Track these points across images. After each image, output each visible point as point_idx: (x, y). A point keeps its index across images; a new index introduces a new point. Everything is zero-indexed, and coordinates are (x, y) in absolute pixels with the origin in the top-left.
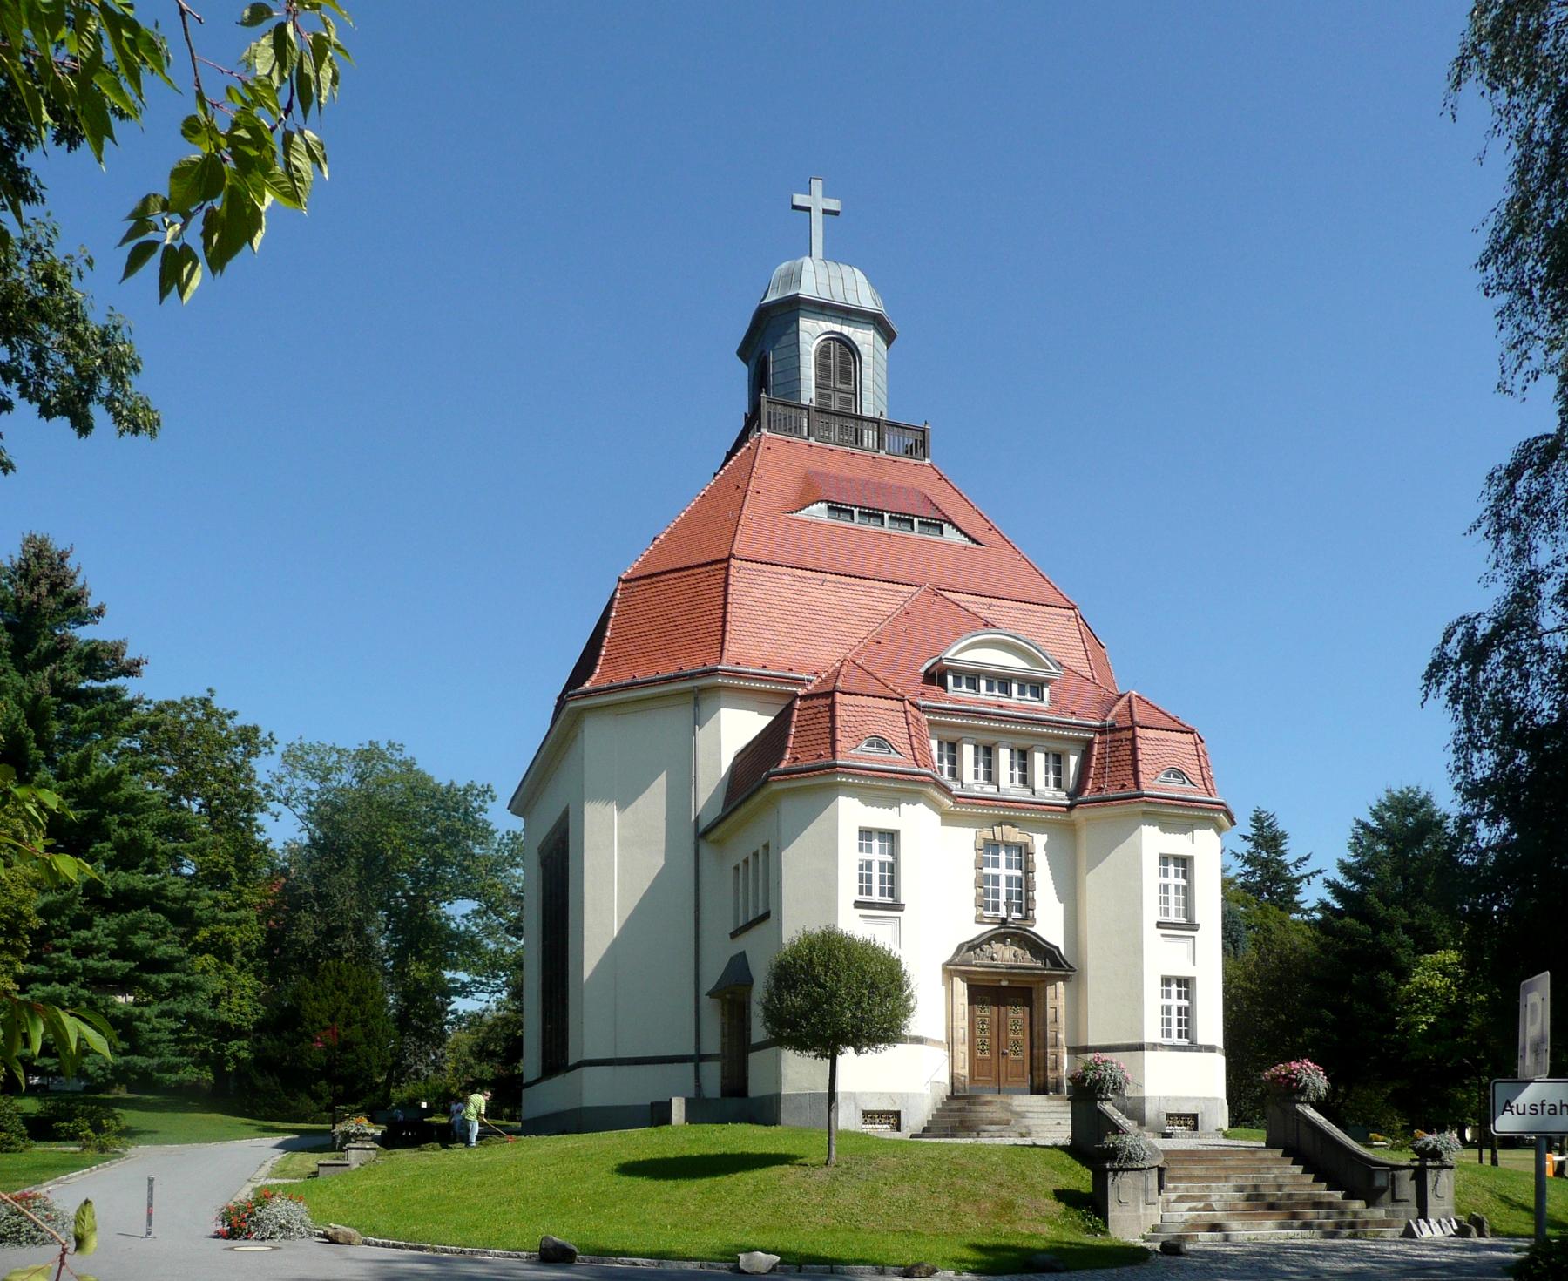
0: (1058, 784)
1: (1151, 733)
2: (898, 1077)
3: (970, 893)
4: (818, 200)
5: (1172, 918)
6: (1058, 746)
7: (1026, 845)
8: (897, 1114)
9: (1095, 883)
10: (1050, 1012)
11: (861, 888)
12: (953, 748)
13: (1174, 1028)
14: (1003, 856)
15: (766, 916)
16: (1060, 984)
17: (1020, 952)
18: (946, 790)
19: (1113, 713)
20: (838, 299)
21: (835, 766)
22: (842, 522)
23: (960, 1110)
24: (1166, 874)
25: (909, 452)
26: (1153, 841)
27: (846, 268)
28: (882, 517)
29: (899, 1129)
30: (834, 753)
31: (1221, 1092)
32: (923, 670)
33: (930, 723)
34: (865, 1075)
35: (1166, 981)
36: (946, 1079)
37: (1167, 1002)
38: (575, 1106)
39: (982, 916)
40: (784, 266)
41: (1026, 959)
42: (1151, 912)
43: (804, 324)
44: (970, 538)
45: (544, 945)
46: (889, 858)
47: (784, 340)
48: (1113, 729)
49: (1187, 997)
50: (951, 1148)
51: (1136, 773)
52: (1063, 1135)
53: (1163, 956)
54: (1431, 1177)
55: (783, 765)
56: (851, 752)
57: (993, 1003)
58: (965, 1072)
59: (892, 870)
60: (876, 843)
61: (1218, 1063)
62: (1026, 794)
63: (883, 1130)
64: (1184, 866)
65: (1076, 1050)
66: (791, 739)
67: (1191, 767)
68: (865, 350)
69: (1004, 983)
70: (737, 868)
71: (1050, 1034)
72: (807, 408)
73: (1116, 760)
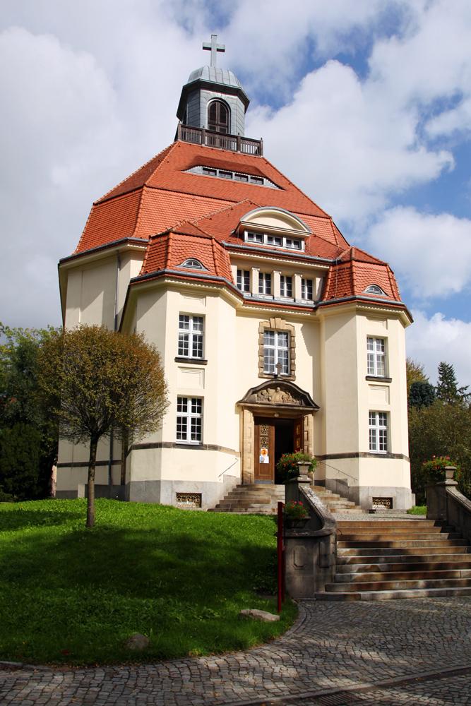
0: (310, 297)
3: (256, 359)
7: (290, 331)
8: (200, 495)
16: (310, 416)
18: (240, 296)
20: (220, 81)
24: (371, 348)
26: (363, 326)
29: (200, 506)
31: (407, 483)
35: (372, 414)
36: (239, 476)
37: (373, 427)
41: (291, 401)
42: (362, 371)
44: (278, 186)
48: (340, 262)
49: (385, 424)
51: (352, 286)
53: (371, 398)
58: (252, 470)
59: (199, 340)
60: (191, 322)
61: (405, 466)
63: (189, 505)
64: (383, 343)
67: (385, 284)
69: (276, 416)
73: (341, 280)
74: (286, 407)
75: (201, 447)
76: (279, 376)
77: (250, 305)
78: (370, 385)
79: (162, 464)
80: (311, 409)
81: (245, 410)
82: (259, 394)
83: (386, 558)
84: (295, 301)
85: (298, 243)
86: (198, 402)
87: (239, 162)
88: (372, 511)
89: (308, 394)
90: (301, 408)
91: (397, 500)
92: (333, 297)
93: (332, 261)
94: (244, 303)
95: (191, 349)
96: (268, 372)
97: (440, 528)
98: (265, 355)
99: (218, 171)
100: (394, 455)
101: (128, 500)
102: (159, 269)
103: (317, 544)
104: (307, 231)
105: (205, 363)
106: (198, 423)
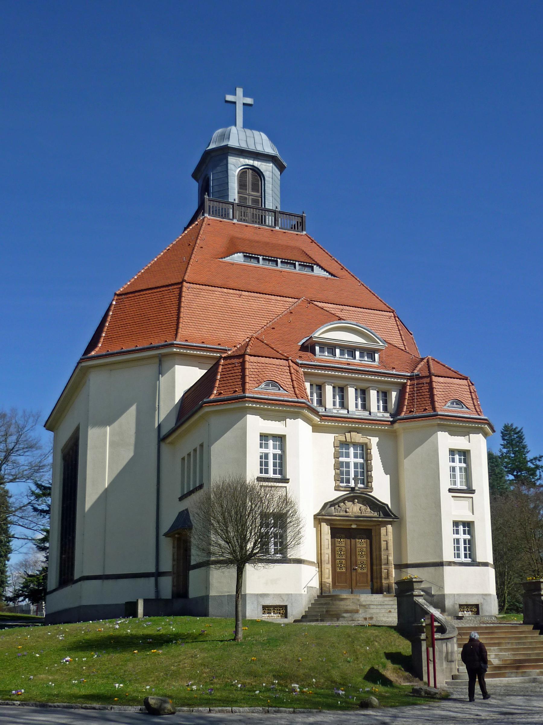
0: (385, 409)
1: (441, 380)
2: (287, 582)
3: (332, 473)
4: (239, 98)
5: (458, 486)
6: (384, 387)
7: (366, 444)
8: (286, 607)
9: (408, 465)
10: (383, 544)
11: (261, 469)
12: (320, 388)
13: (462, 552)
14: (352, 450)
15: (201, 487)
16: (389, 527)
17: (363, 507)
18: (316, 413)
19: (418, 369)
20: (252, 148)
21: (245, 397)
22: (253, 263)
23: (326, 604)
25: (293, 228)
26: (445, 441)
27: (256, 133)
28: (277, 261)
29: (286, 617)
30: (244, 391)
31: (492, 589)
32: (300, 344)
33: (305, 373)
34: (263, 581)
35: (456, 524)
38: (76, 604)
39: (339, 486)
40: (220, 131)
41: (368, 512)
43: (232, 160)
44: (330, 273)
45: (63, 507)
46: (278, 452)
47: (219, 169)
48: (418, 377)
50: (322, 628)
51: (433, 402)
52: (393, 619)
55: (212, 397)
56: (254, 389)
57: (346, 537)
60: (271, 443)
61: (491, 572)
62: (365, 414)
63: (275, 618)
64: (465, 456)
65: (400, 567)
66: (218, 382)
68: (267, 174)
69: (354, 526)
70: (183, 459)
71: (383, 557)
72: (233, 204)
74: (365, 519)
75: (285, 560)
76: (357, 488)
78: (453, 497)
80: (391, 520)
82: (337, 506)
84: (370, 414)
85: (371, 357)
87: (280, 242)
88: (460, 618)
89: (387, 505)
90: (380, 519)
92: (411, 412)
93: (409, 374)
95: (271, 468)
97: (539, 631)
98: (341, 470)
99: (261, 258)
100: (479, 563)
101: (206, 614)
104: (381, 344)
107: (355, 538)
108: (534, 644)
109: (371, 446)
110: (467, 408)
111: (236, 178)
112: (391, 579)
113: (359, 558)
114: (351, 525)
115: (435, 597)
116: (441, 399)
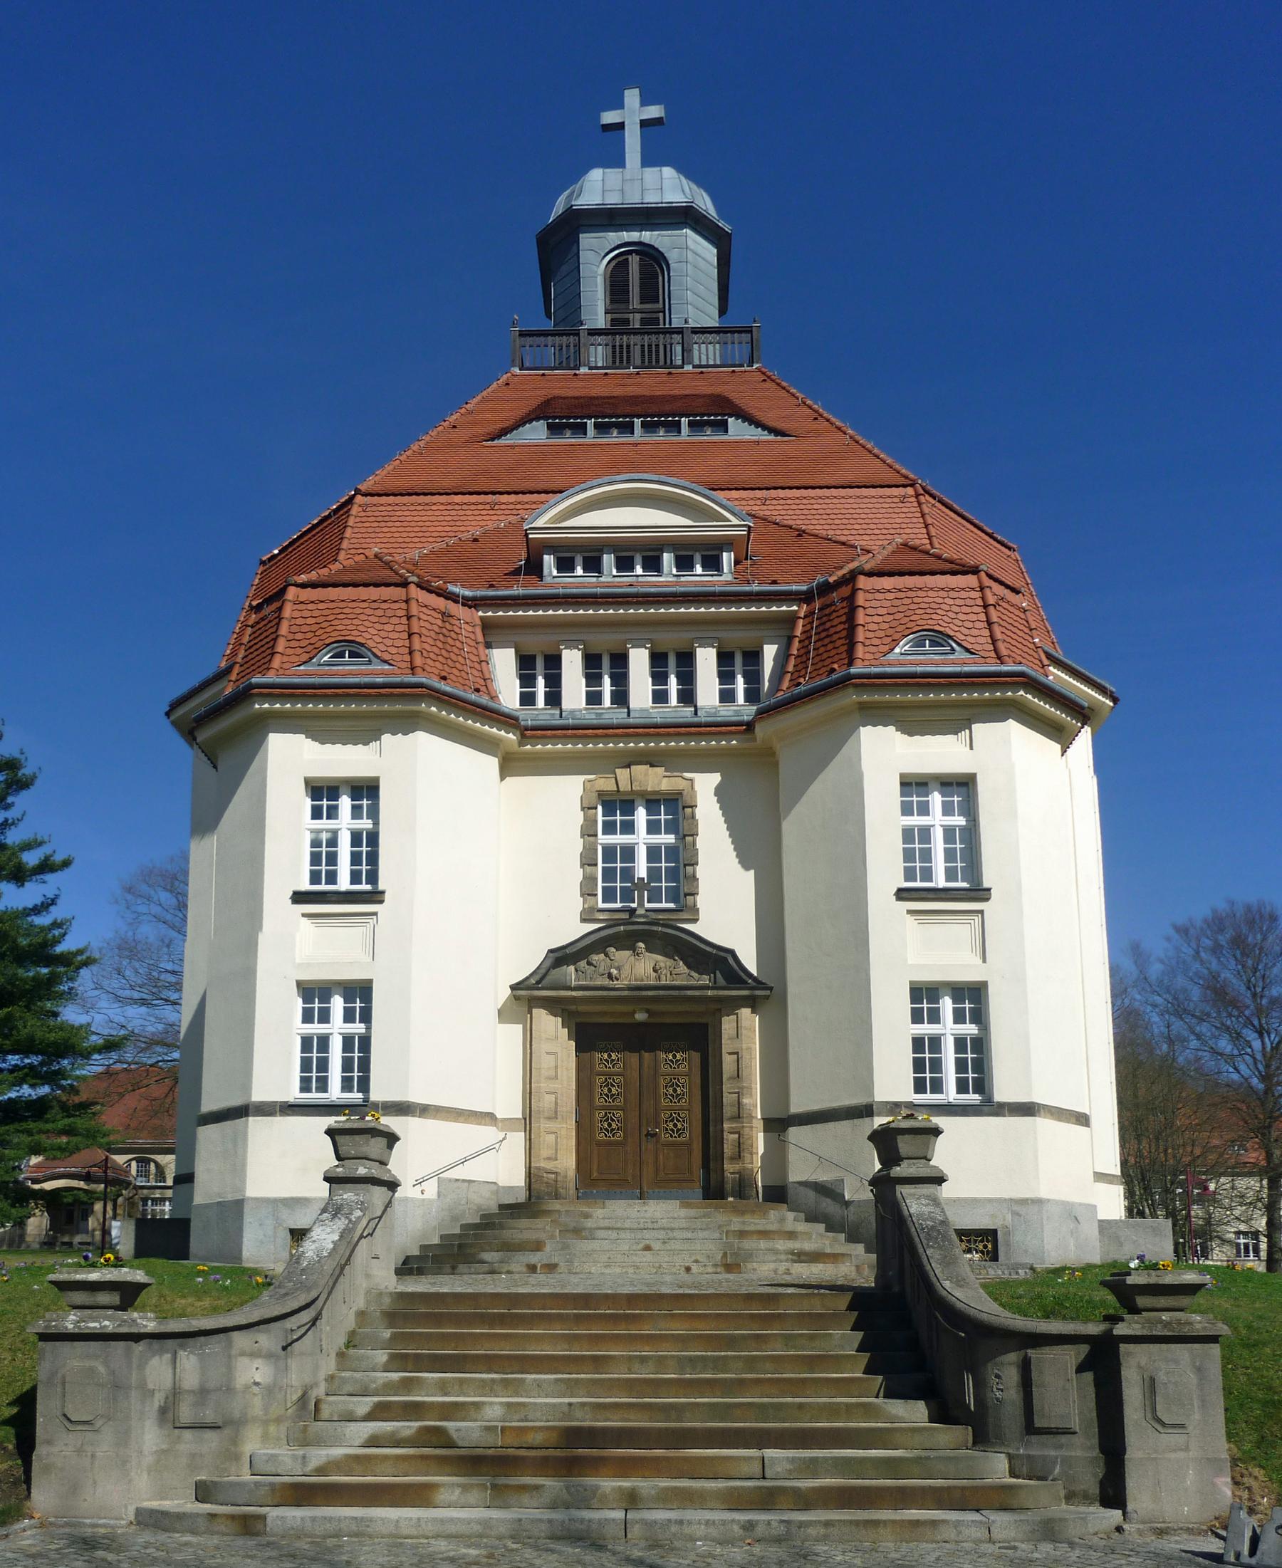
16: (745, 1012)
26: (885, 753)
33: (487, 625)
41: (676, 973)
42: (884, 869)
43: (588, 241)
44: (772, 430)
48: (825, 588)
54: (1135, 1365)
69: (640, 1017)
77: (535, 739)
78: (909, 912)
79: (249, 1160)
81: (535, 1011)
82: (583, 964)
83: (509, 1405)
84: (696, 713)
86: (972, 998)
91: (1017, 1238)
93: (804, 588)
94: (523, 736)
96: (618, 905)
102: (833, 670)
103: (168, 1356)
104: (735, 521)
105: (378, 898)
106: (359, 1048)
107: (652, 1049)
108: (768, 1365)
109: (694, 796)
110: (968, 650)
111: (600, 281)
112: (747, 1159)
113: (664, 1103)
114: (634, 1012)
115: (851, 1208)
116: (881, 634)
